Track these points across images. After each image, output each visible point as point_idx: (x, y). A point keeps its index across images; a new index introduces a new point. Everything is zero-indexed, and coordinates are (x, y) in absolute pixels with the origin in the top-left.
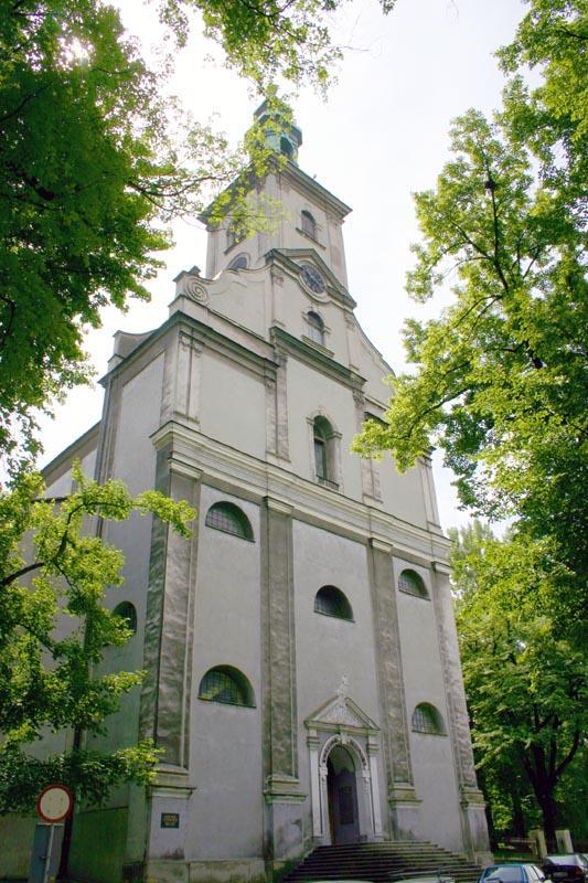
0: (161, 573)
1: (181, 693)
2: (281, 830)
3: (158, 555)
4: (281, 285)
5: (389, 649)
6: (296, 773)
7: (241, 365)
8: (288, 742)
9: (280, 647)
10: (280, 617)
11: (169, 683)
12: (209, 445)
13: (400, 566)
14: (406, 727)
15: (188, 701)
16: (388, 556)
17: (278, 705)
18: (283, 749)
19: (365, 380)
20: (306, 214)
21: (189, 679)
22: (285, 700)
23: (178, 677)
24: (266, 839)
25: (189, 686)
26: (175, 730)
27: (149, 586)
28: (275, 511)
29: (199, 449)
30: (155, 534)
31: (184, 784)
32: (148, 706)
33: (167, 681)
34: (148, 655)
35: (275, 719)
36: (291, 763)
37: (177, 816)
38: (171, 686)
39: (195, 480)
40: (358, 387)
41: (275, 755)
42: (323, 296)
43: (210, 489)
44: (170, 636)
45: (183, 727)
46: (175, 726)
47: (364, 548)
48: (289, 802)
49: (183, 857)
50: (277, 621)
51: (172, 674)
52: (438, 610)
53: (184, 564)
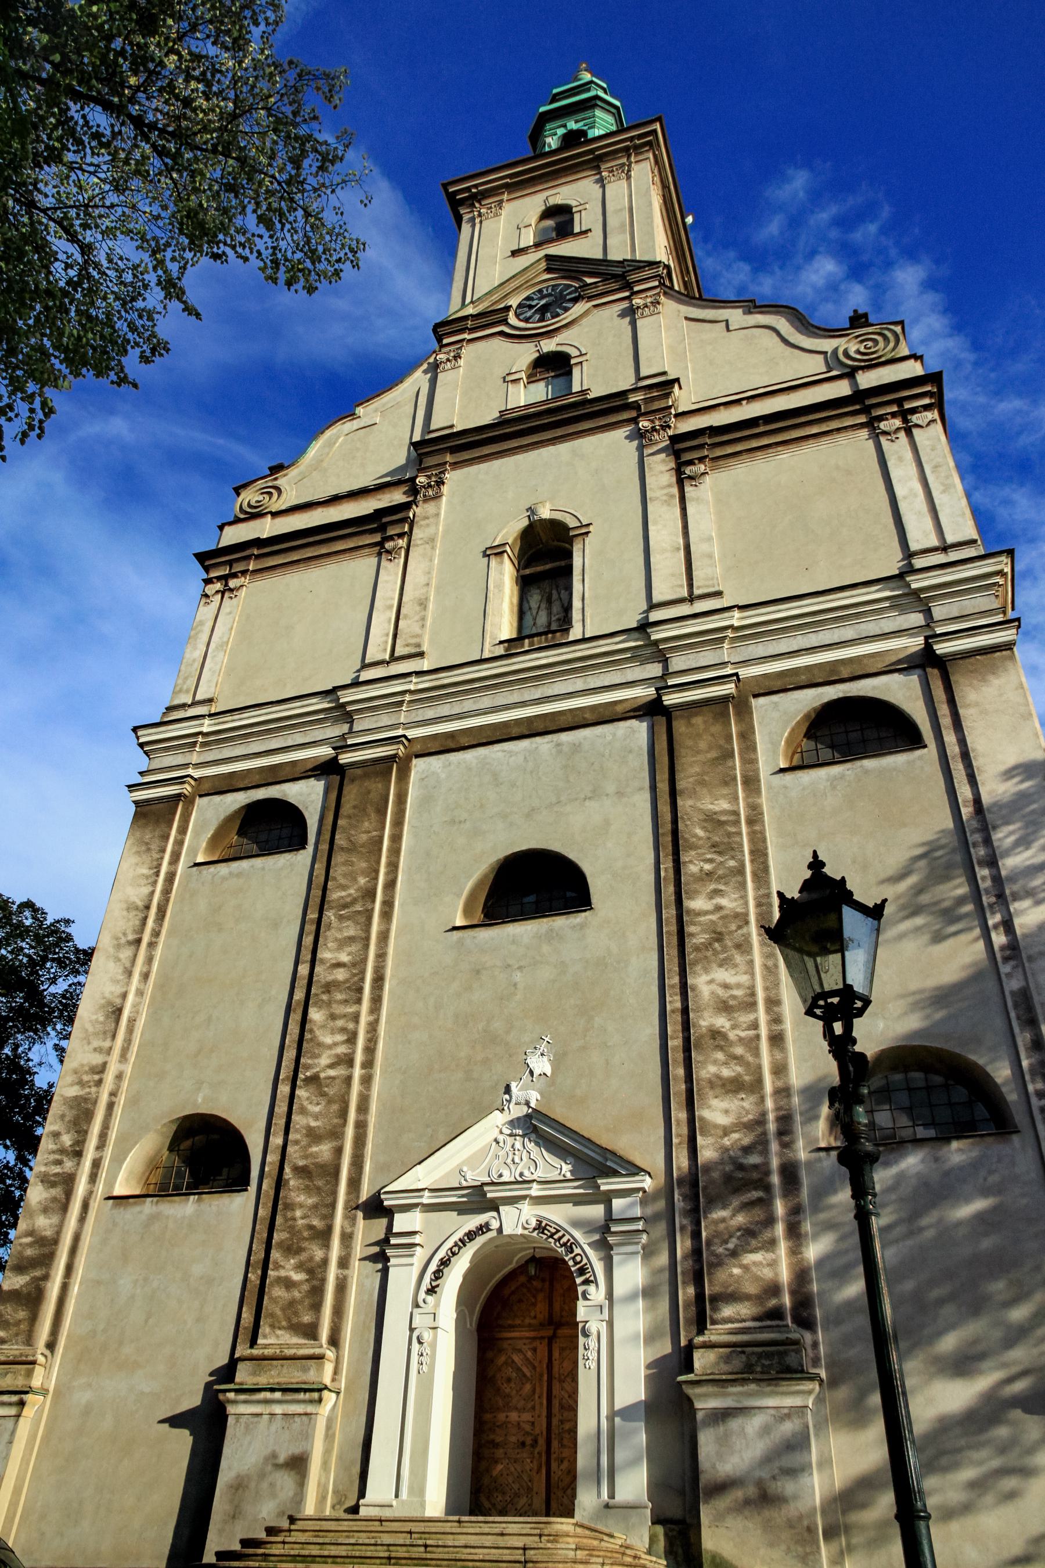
7: (838, 430)
26: (38, 1273)
35: (290, 1207)
38: (53, 1185)
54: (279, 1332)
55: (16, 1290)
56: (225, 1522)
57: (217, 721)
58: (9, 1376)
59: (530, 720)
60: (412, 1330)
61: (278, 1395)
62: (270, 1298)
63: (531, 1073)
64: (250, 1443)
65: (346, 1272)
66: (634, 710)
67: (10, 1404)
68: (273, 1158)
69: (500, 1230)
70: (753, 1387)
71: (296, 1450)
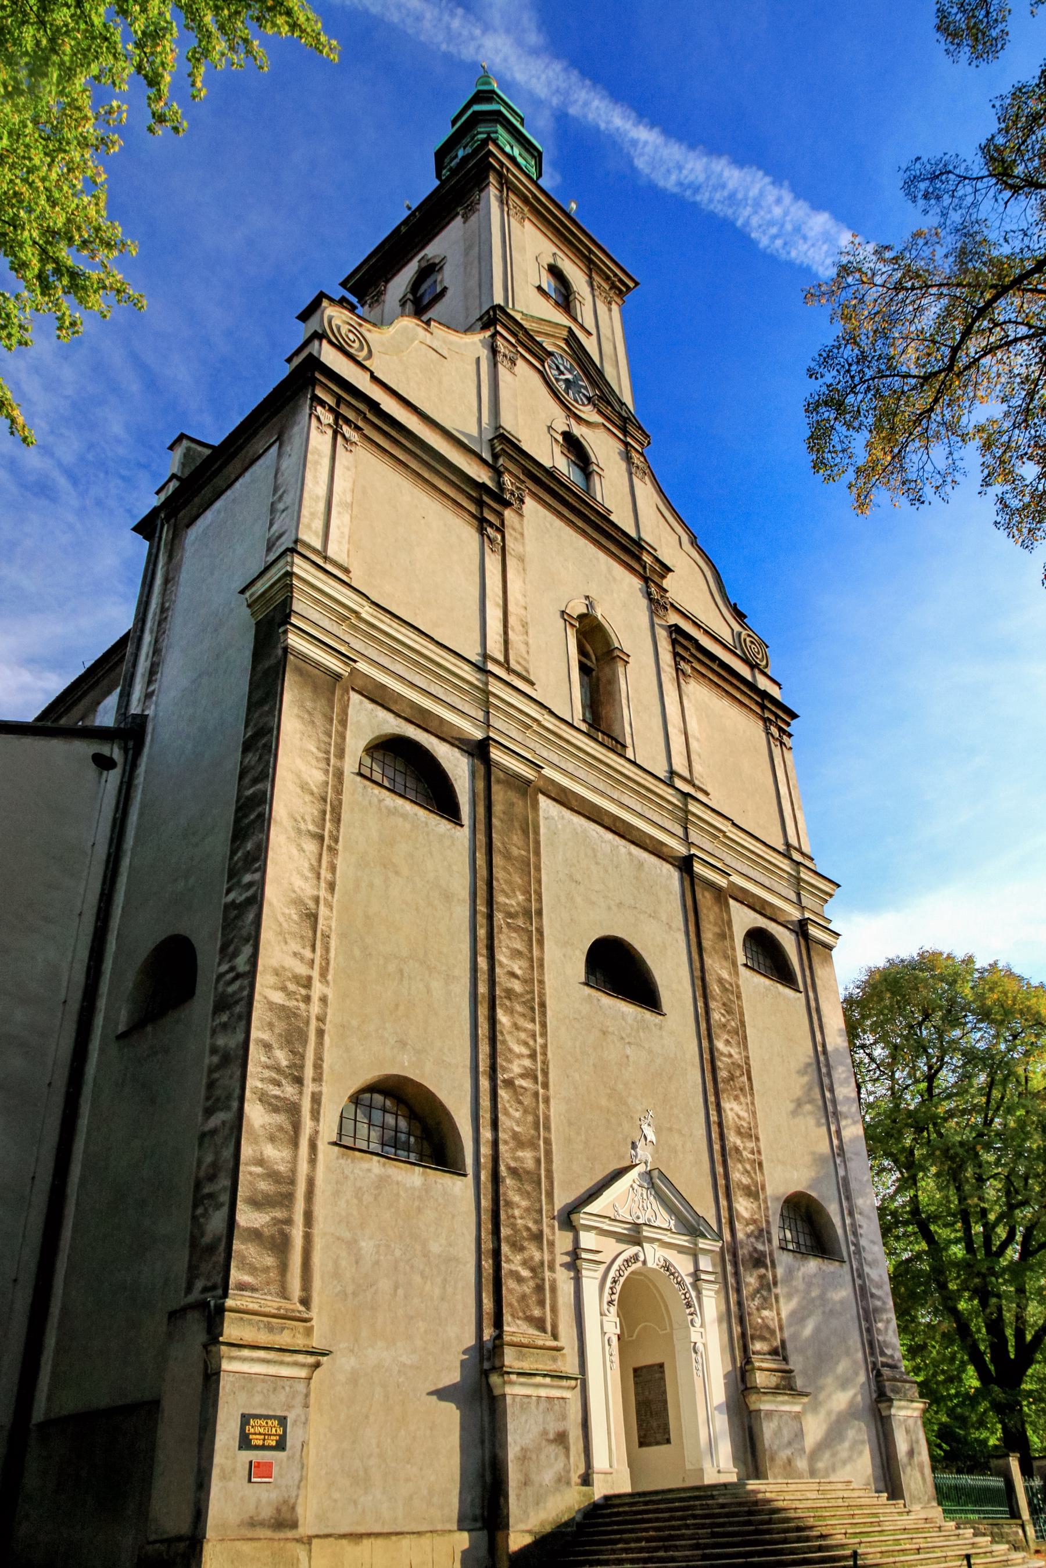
0: (257, 859)
1: (296, 1127)
2: (524, 1457)
3: (253, 822)
4: (510, 369)
5: (732, 1078)
6: (554, 1327)
7: (426, 481)
8: (537, 1256)
9: (518, 1049)
10: (517, 986)
11: (273, 1105)
12: (366, 611)
13: (743, 919)
14: (770, 1241)
15: (313, 1147)
16: (721, 895)
17: (514, 1172)
18: (525, 1273)
19: (669, 570)
20: (554, 271)
21: (316, 1099)
22: (530, 1164)
23: (289, 1090)
24: (488, 1478)
25: (316, 1115)
26: (279, 1214)
27: (228, 891)
28: (505, 770)
29: (347, 616)
30: (247, 780)
31: (300, 1342)
32: (217, 1154)
33: (263, 1098)
34: (221, 1041)
35: (509, 1204)
36: (541, 1303)
37: (282, 1421)
38: (276, 1110)
39: (338, 677)
40: (656, 578)
41: (509, 1284)
42: (589, 413)
43: (369, 705)
44: (278, 997)
45: (300, 1206)
46: (281, 1204)
47: (675, 875)
48: (543, 1392)
49: (294, 1525)
50: (509, 993)
51: (279, 1084)
52: (814, 1013)
53: (311, 847)
54: (519, 1322)
55: (256, 1229)
56: (520, 1488)
57: (375, 613)
58: (286, 1332)
59: (617, 818)
60: (604, 1333)
61: (548, 1380)
62: (507, 1289)
63: (646, 1138)
64: (526, 1421)
65: (554, 1275)
66: (459, 739)
67: (303, 1365)
68: (485, 1150)
69: (644, 1262)
70: (786, 1398)
71: (560, 1427)
